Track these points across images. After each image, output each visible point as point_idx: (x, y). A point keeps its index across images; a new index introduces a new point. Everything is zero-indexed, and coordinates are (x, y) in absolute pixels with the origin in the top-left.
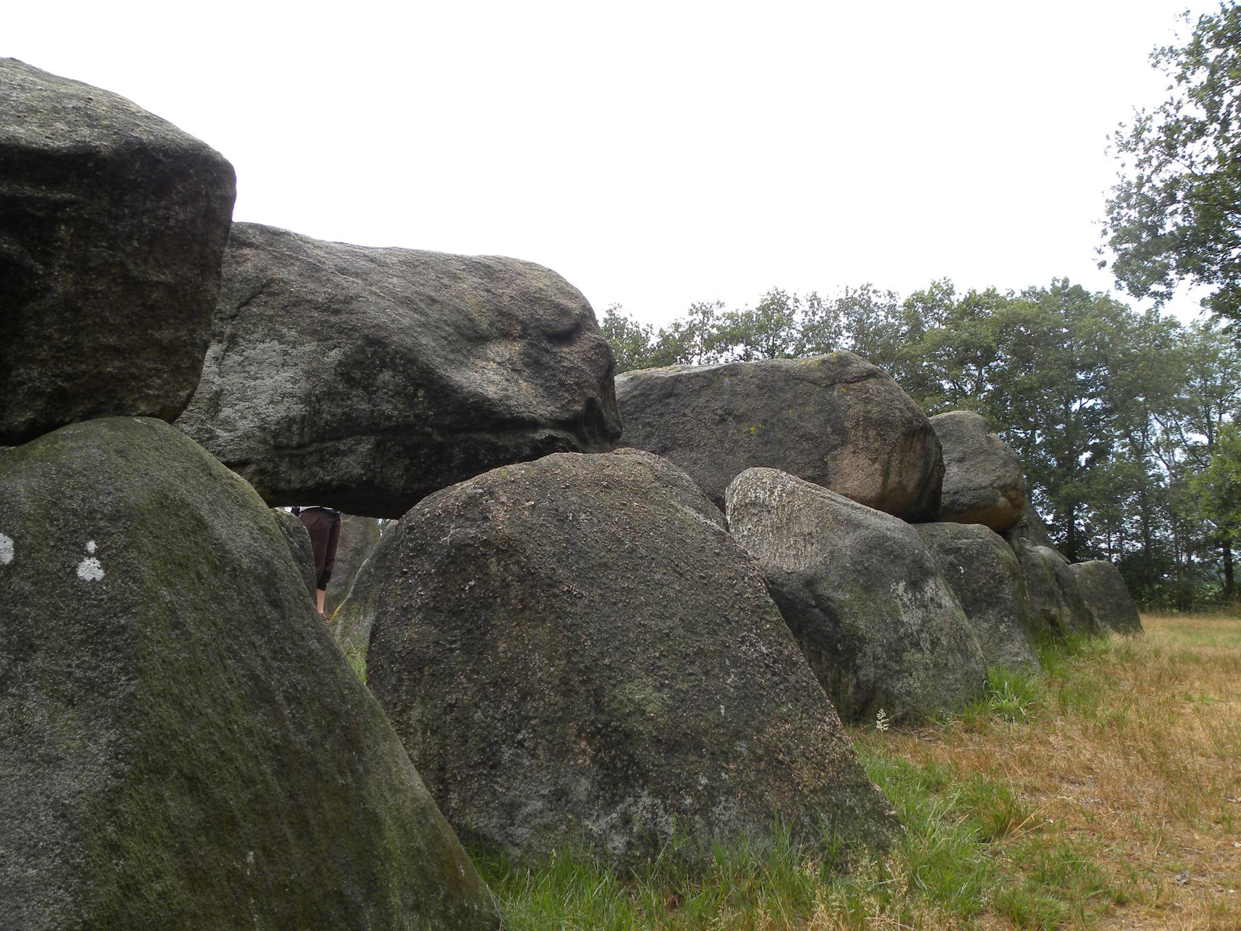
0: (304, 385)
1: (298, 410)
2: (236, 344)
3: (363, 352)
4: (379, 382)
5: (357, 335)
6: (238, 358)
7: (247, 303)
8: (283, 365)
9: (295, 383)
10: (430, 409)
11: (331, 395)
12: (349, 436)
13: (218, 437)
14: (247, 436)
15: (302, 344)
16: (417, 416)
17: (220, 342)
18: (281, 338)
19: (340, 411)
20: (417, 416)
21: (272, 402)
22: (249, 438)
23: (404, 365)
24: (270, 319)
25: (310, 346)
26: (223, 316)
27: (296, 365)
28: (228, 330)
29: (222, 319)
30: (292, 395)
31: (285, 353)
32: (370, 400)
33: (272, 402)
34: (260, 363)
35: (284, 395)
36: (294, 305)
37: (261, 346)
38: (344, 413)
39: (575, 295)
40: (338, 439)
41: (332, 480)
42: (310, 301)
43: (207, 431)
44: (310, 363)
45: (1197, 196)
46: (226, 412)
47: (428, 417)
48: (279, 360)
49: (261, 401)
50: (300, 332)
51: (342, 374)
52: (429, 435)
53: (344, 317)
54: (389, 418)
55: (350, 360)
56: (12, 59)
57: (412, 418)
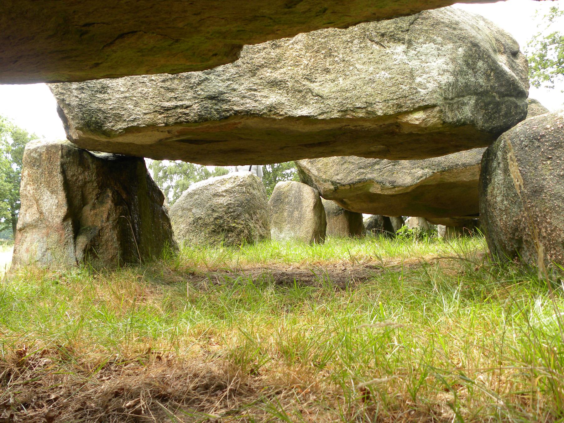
0: (451, 67)
1: (451, 79)
2: (411, 44)
3: (471, 50)
4: (478, 67)
5: (466, 41)
6: (414, 52)
7: (412, 23)
8: (438, 56)
9: (447, 64)
10: (496, 83)
11: (461, 72)
12: (467, 95)
13: (420, 92)
14: (434, 92)
15: (446, 45)
16: (491, 86)
17: (403, 43)
18: (434, 41)
19: (464, 81)
20: (491, 86)
21: (439, 74)
22: (435, 92)
23: (487, 58)
24: (426, 31)
25: (450, 46)
26: (402, 29)
27: (445, 55)
28: (407, 37)
29: (402, 31)
30: (448, 71)
31: (438, 49)
32: (475, 76)
33: (439, 74)
34: (426, 55)
35: (444, 71)
36: (436, 24)
37: (425, 46)
38: (466, 83)
39: (515, 42)
40: (463, 96)
41: (462, 118)
42: (443, 23)
43: (414, 89)
44: (451, 54)
45: (94, 254)
46: (418, 80)
47: (495, 87)
48: (436, 52)
49: (435, 73)
50: (443, 38)
51: (465, 61)
52: (494, 97)
53: (459, 32)
54: (481, 86)
55: (467, 54)
56: (61, 112)
57: (489, 87)
